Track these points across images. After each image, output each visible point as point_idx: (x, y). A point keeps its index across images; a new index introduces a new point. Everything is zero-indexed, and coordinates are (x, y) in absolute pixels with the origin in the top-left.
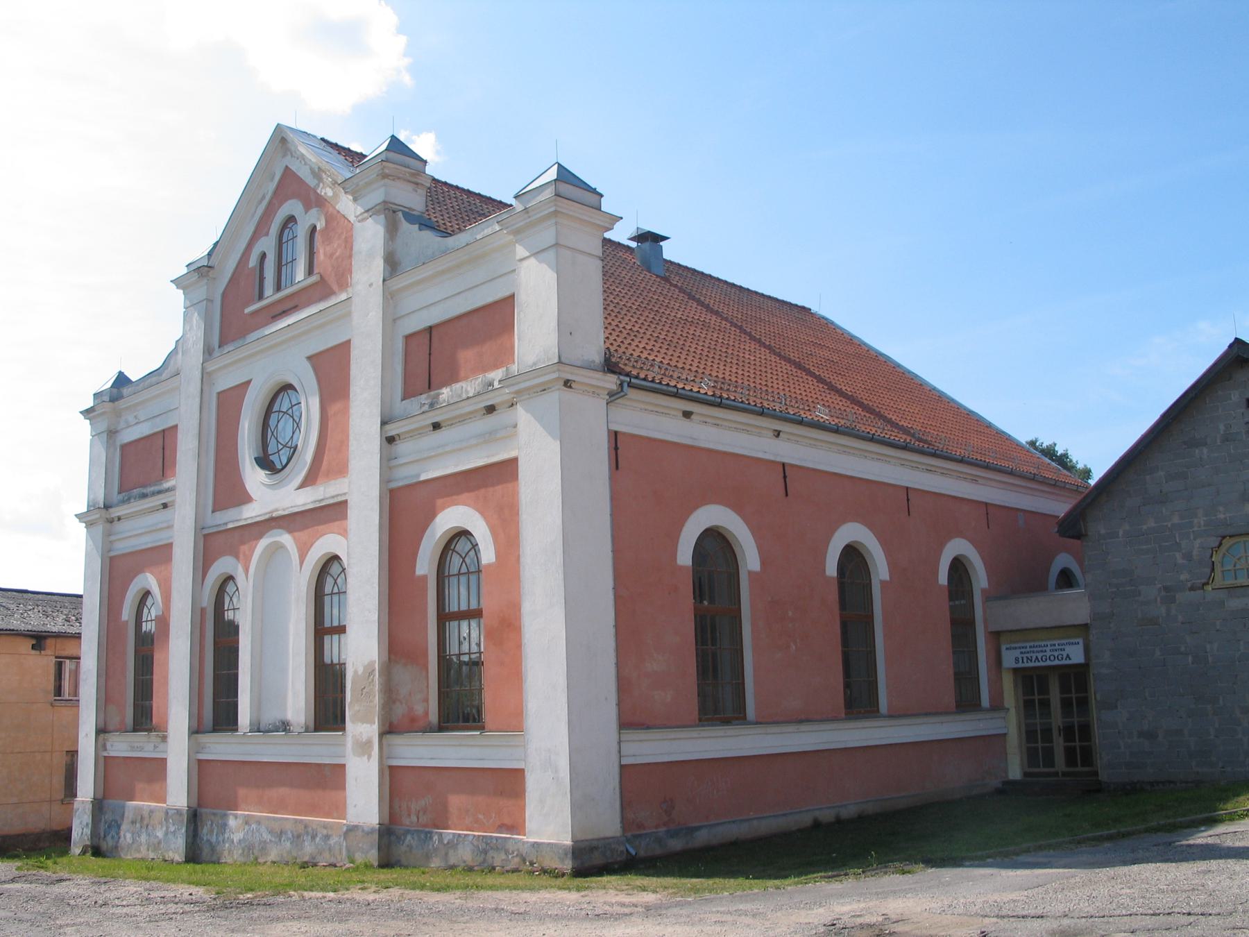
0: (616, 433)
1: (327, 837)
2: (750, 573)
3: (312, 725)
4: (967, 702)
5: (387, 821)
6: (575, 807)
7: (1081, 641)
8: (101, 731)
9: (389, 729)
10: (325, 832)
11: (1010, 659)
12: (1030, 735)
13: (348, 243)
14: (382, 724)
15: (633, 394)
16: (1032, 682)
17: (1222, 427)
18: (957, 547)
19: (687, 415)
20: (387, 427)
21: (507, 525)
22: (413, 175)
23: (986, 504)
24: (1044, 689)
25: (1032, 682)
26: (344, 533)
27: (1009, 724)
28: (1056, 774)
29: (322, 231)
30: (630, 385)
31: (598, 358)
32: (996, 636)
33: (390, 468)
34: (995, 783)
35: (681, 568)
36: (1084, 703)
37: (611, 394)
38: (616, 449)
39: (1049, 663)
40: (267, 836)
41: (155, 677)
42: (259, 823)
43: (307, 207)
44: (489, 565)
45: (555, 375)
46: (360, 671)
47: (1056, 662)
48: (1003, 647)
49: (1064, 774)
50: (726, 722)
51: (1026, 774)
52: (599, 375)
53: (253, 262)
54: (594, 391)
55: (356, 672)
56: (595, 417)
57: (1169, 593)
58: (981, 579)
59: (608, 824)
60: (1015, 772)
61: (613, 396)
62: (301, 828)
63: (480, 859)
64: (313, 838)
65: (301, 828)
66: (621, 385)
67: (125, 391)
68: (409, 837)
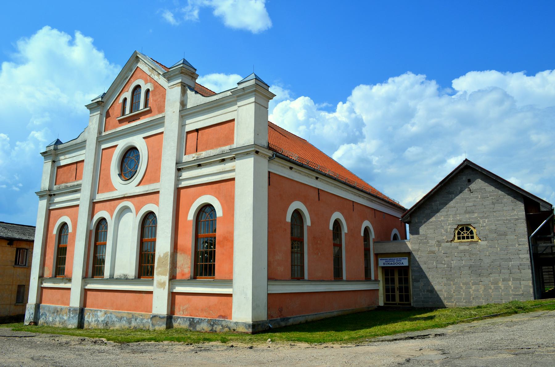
1: (142, 319)
2: (308, 226)
3: (137, 276)
4: (367, 278)
5: (169, 314)
6: (254, 309)
7: (407, 258)
8: (41, 277)
9: (173, 278)
10: (141, 317)
11: (381, 263)
12: (387, 290)
13: (164, 96)
14: (170, 276)
15: (277, 159)
16: (388, 271)
17: (459, 188)
19: (291, 168)
20: (178, 165)
21: (229, 203)
22: (191, 73)
24: (393, 275)
25: (388, 271)
26: (157, 203)
27: (381, 287)
28: (396, 304)
29: (152, 91)
30: (276, 156)
31: (266, 145)
32: (377, 255)
33: (178, 180)
34: (375, 306)
35: (287, 223)
36: (407, 280)
37: (270, 158)
39: (395, 265)
40: (115, 319)
41: (67, 256)
42: (111, 313)
43: (146, 82)
44: (220, 217)
45: (253, 149)
46: (162, 255)
47: (398, 265)
48: (379, 259)
49: (399, 304)
50: (298, 279)
51: (385, 304)
52: (267, 150)
54: (264, 156)
55: (160, 256)
56: (265, 166)
57: (439, 243)
58: (372, 236)
59: (263, 316)
60: (381, 303)
62: (131, 316)
63: (210, 328)
64: (136, 320)
65: (131, 316)
66: (273, 155)
67: (60, 147)
68: (179, 320)
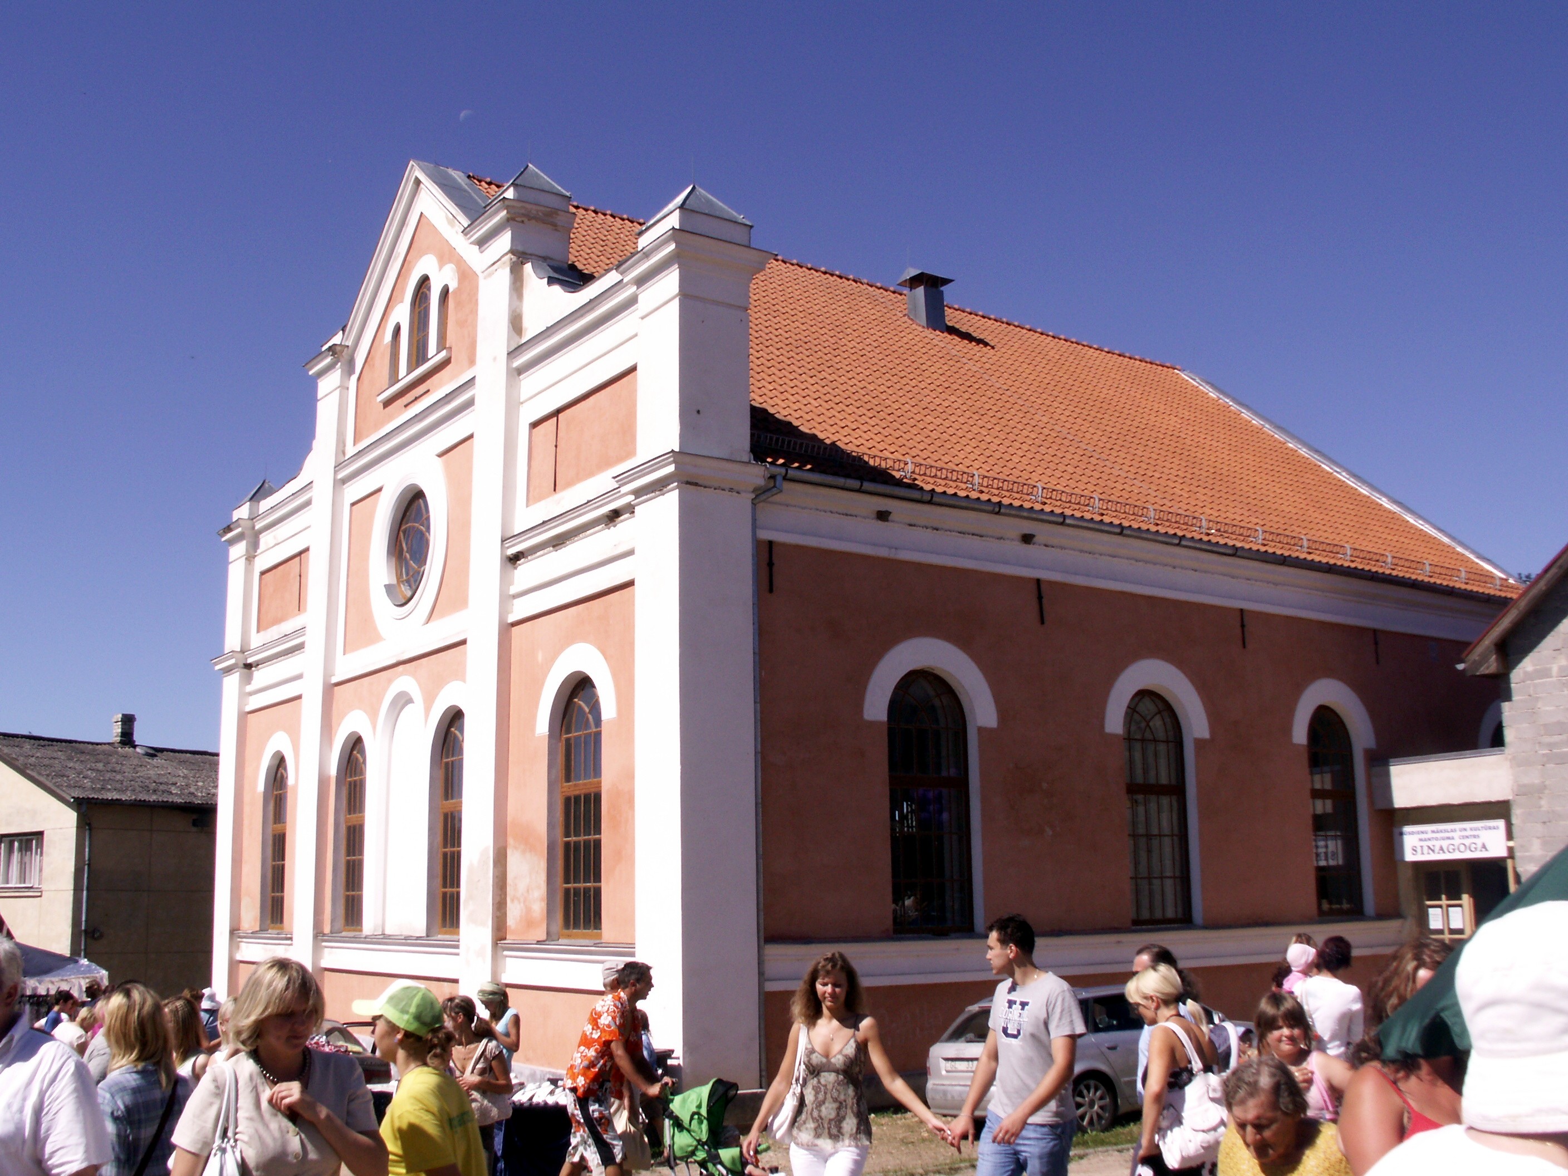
0: (770, 543)
2: (981, 730)
18: (1327, 692)
23: (1375, 631)
29: (455, 292)
38: (770, 564)
53: (388, 337)
61: (760, 494)
